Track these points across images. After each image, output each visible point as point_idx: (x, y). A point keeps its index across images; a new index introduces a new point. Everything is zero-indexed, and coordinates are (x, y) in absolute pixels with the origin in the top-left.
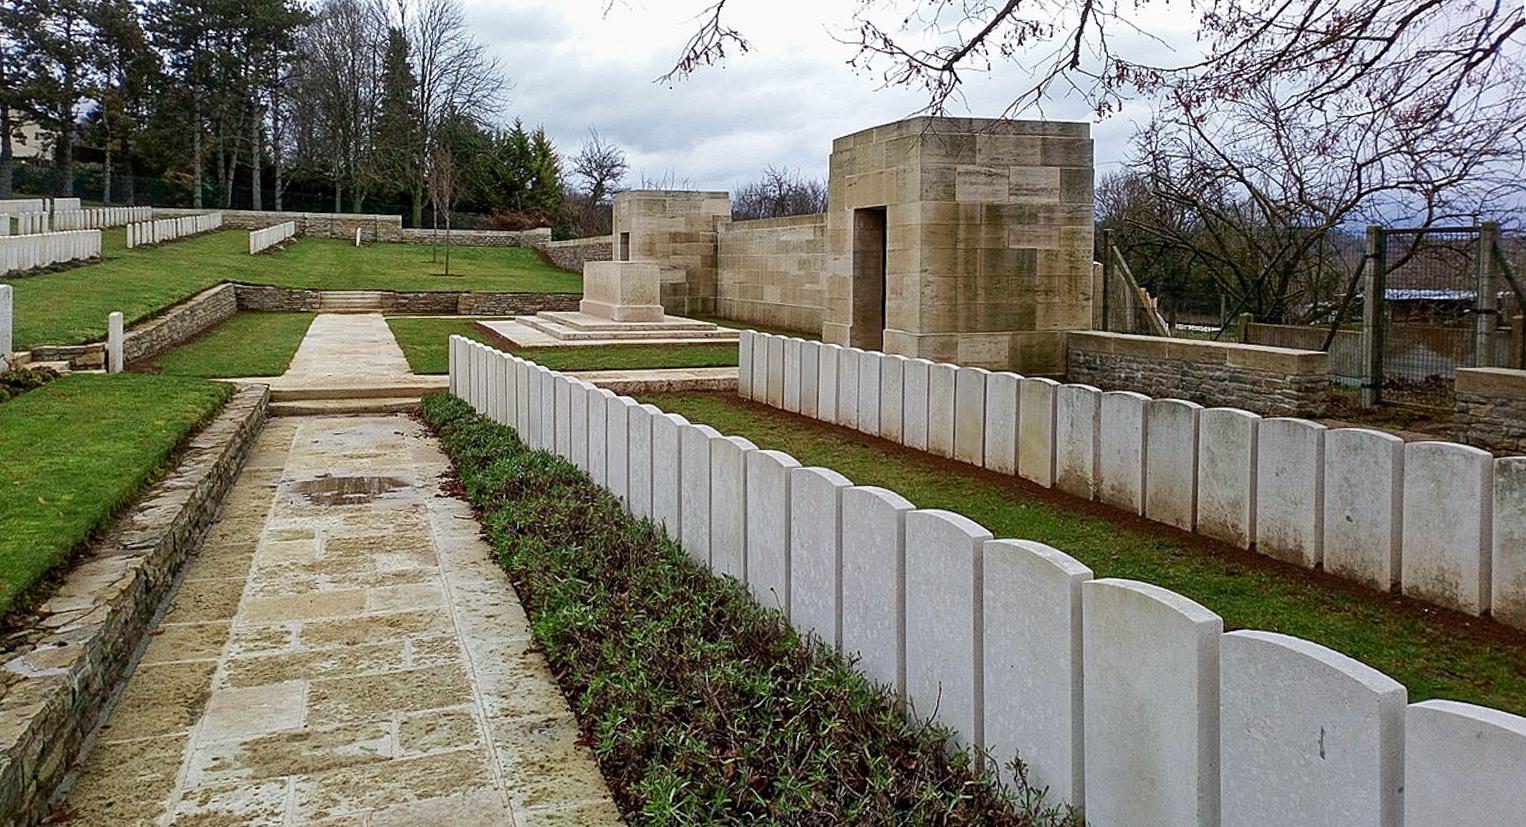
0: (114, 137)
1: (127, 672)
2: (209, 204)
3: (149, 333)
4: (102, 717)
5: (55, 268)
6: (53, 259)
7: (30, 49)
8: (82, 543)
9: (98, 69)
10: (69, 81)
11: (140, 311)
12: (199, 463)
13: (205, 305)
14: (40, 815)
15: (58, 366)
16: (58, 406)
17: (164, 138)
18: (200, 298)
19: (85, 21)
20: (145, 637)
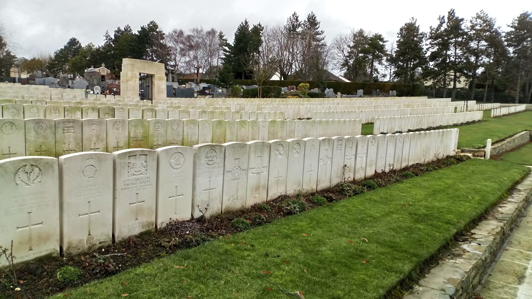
0: (489, 80)
1: (496, 259)
2: (521, 102)
3: (498, 147)
4: (489, 271)
5: (468, 123)
6: (467, 121)
7: (465, 53)
8: (482, 214)
9: (487, 57)
10: (477, 62)
11: (496, 139)
12: (520, 194)
13: (518, 138)
14: (472, 295)
15: (470, 155)
16: (471, 168)
17: (507, 79)
18: (517, 136)
19: (484, 41)
20: (502, 250)
